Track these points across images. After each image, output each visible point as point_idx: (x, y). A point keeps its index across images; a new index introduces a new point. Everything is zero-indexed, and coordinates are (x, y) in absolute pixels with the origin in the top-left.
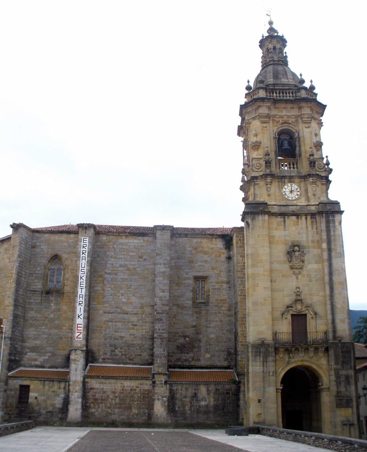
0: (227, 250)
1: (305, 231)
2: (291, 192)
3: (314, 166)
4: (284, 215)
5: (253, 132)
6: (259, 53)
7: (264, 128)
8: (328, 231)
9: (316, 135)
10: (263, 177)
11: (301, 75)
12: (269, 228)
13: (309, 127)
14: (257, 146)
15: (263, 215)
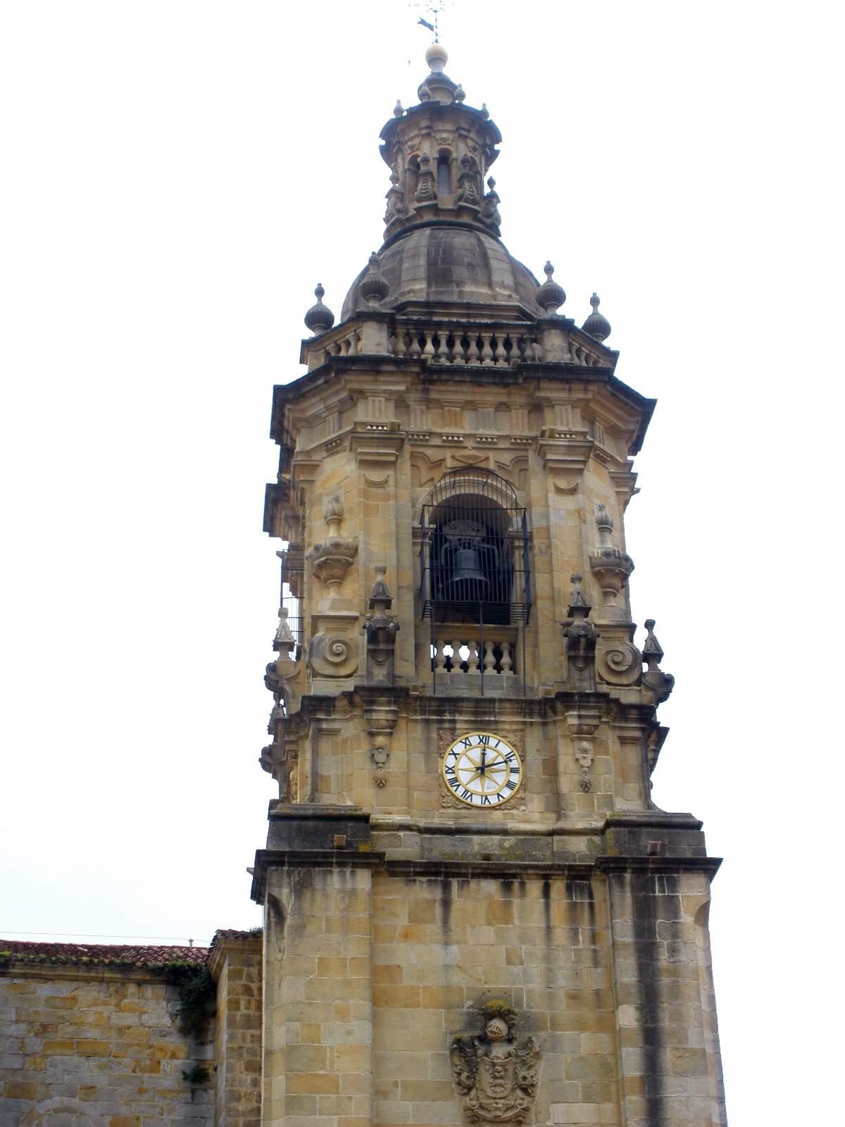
0: (189, 1040)
1: (540, 949)
2: (482, 772)
3: (590, 660)
4: (447, 875)
5: (326, 506)
6: (377, 180)
8: (646, 950)
9: (604, 526)
10: (357, 699)
11: (549, 270)
12: (375, 933)
13: (573, 491)
14: (336, 565)
15: (348, 871)
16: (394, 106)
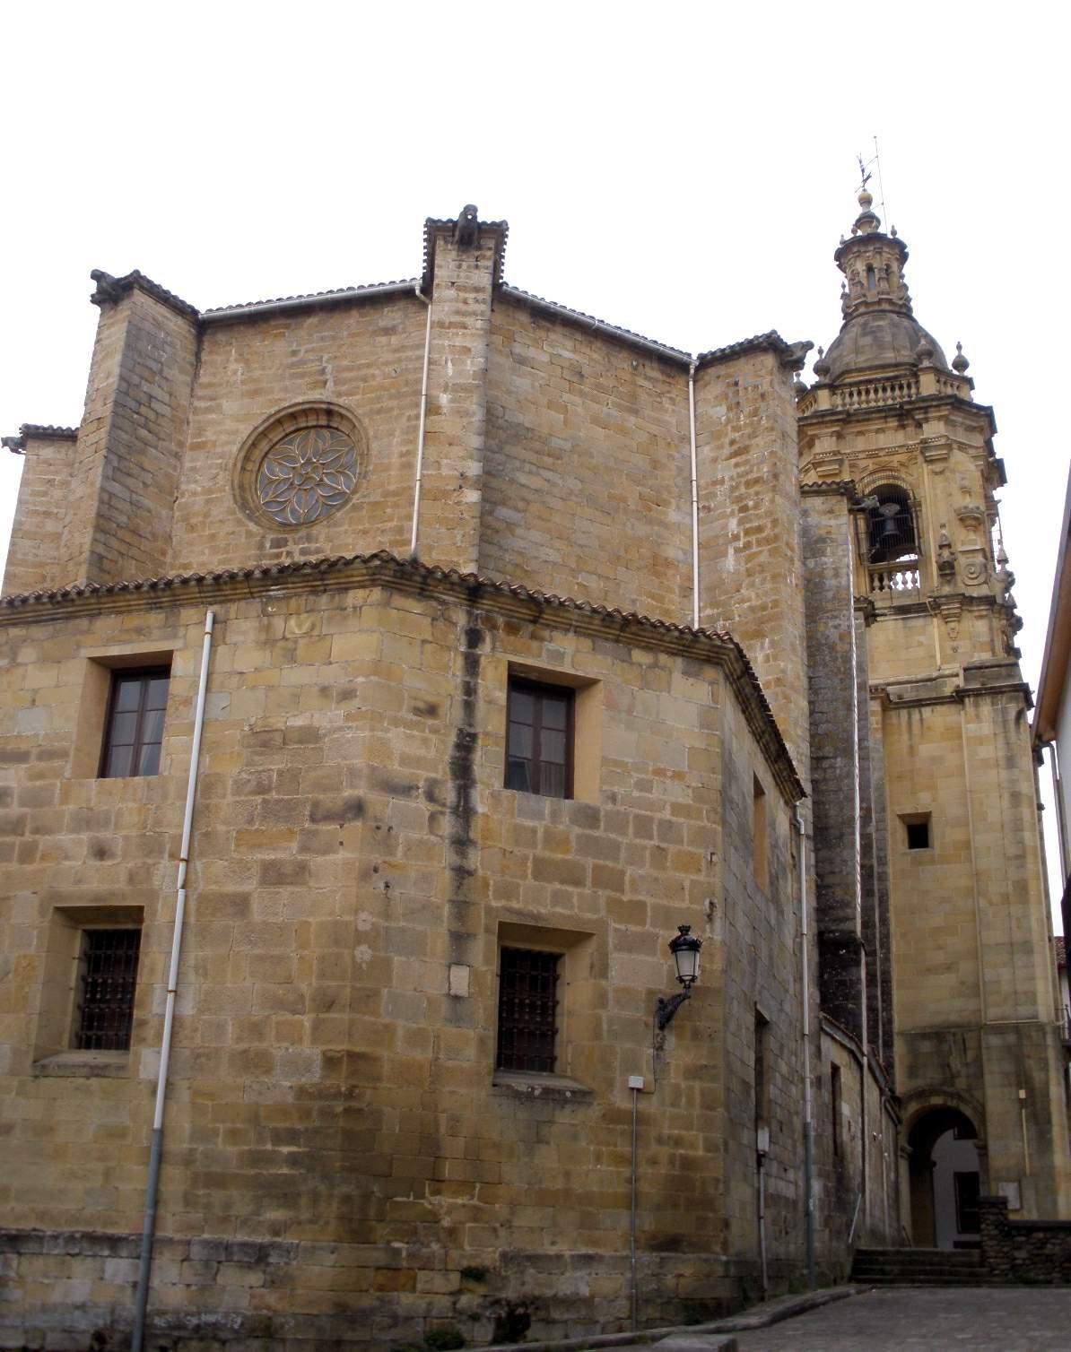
16: (839, 239)
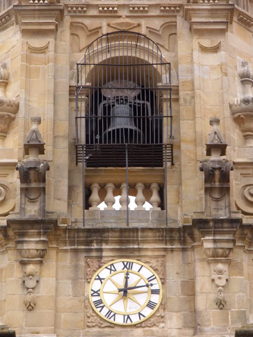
7: (35, 55)
10: (11, 233)
13: (216, 49)
